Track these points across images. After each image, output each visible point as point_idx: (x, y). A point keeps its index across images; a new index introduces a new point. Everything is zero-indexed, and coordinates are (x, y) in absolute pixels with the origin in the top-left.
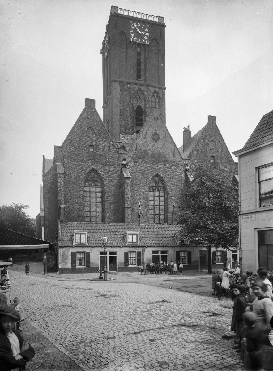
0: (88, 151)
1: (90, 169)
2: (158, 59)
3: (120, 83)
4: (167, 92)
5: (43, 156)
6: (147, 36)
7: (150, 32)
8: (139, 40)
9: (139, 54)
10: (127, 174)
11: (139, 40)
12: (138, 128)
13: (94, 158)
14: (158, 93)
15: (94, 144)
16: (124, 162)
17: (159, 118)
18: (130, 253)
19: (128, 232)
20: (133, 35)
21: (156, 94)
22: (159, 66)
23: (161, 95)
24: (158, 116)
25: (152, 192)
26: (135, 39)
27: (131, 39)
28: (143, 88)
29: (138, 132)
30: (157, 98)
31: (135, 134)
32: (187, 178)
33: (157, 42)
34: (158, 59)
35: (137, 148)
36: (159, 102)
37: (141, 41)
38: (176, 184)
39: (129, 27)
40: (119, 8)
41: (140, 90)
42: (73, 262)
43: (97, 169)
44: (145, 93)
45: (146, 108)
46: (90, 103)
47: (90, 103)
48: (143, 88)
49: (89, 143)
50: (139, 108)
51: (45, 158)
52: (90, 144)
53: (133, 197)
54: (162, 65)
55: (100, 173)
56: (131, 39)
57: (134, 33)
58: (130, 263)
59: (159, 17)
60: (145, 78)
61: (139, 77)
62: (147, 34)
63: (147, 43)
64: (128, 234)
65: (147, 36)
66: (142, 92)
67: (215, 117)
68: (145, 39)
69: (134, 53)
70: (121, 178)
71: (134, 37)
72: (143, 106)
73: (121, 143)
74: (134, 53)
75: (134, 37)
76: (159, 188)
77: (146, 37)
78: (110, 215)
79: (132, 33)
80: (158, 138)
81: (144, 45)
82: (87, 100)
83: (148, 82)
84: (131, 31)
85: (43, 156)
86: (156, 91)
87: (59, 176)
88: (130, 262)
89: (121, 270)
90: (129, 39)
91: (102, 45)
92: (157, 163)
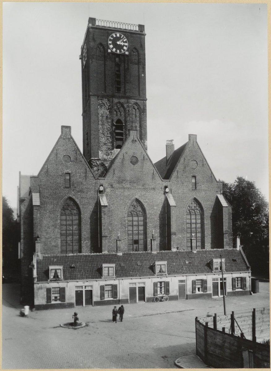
0: (65, 179)
1: (66, 197)
2: (139, 68)
3: (98, 97)
4: (148, 103)
5: (20, 173)
6: (126, 46)
7: (129, 41)
8: (118, 51)
9: (118, 65)
10: (104, 201)
12: (120, 143)
13: (70, 186)
14: (139, 105)
15: (70, 172)
16: (101, 188)
17: (137, 140)
18: (106, 287)
19: (104, 265)
20: (111, 46)
21: (137, 106)
22: (139, 76)
23: (142, 107)
24: (136, 139)
25: (130, 217)
26: (114, 50)
27: (109, 51)
28: (122, 101)
29: (119, 147)
30: (138, 110)
31: (115, 149)
32: (166, 200)
33: (137, 51)
34: (139, 68)
35: (114, 173)
36: (140, 114)
37: (120, 51)
38: (155, 208)
39: (108, 38)
40: (97, 20)
41: (119, 102)
42: (49, 298)
43: (74, 197)
44: (125, 106)
45: (126, 122)
46: (66, 129)
47: (66, 129)
49: (66, 171)
50: (119, 121)
51: (22, 174)
52: (67, 172)
53: (111, 224)
54: (143, 75)
55: (77, 200)
56: (109, 51)
57: (113, 44)
58: (105, 297)
59: (139, 25)
60: (125, 90)
61: (119, 90)
62: (126, 44)
63: (127, 53)
64: (104, 267)
65: (126, 46)
66: (122, 106)
67: (196, 135)
68: (124, 50)
69: (113, 70)
70: (98, 205)
71: (113, 48)
72: (123, 119)
73: (100, 160)
74: (113, 70)
75: (113, 48)
76: (138, 212)
77: (125, 48)
78: (87, 243)
79: (110, 44)
80: (137, 161)
81: (124, 55)
82: (63, 127)
83: (128, 94)
84: (110, 42)
85: (20, 173)
86: (137, 103)
87: (35, 208)
88: (106, 295)
89: (98, 303)
90: (108, 51)
91: (81, 49)
92: (136, 187)
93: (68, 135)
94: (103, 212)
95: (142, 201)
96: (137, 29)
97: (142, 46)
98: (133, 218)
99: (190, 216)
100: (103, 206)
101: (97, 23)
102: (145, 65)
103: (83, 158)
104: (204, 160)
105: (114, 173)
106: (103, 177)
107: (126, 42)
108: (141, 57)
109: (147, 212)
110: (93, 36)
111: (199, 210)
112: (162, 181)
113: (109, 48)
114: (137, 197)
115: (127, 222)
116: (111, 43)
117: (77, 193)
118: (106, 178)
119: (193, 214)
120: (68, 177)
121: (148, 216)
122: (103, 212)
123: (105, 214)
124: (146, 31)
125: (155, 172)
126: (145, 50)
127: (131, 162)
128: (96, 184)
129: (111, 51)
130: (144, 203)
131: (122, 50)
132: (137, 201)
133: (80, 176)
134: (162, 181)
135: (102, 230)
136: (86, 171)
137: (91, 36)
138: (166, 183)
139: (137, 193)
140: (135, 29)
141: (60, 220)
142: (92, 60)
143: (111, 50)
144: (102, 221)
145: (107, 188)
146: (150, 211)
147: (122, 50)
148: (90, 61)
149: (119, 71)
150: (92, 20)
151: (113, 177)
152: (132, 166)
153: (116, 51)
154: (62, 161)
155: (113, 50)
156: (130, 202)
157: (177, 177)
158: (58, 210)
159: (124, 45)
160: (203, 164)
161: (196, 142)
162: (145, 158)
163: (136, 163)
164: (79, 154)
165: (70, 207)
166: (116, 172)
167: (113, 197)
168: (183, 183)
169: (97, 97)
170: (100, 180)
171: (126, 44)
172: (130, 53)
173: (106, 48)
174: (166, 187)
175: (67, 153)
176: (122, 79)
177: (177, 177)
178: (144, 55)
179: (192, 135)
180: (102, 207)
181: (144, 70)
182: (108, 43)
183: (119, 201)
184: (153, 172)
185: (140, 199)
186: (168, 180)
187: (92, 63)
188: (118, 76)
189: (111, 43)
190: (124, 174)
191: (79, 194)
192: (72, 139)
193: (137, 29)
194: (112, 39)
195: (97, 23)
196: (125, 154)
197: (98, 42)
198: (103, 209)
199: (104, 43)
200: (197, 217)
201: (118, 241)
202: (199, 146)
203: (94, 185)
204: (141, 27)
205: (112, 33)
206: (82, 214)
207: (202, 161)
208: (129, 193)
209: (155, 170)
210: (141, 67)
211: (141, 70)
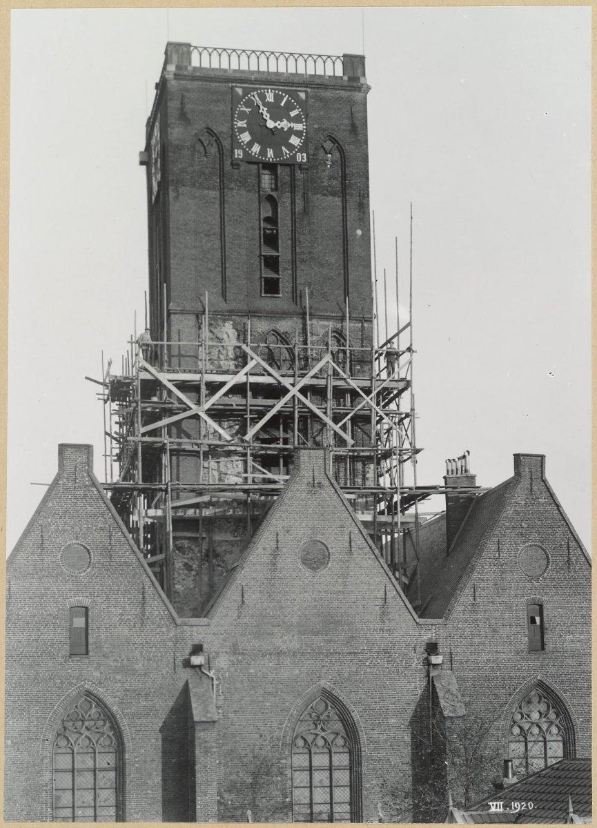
1: (73, 691)
2: (344, 209)
6: (298, 134)
8: (270, 153)
11: (270, 153)
15: (87, 602)
17: (326, 483)
20: (246, 137)
24: (320, 478)
25: (302, 757)
28: (284, 326)
32: (431, 695)
34: (344, 209)
35: (243, 602)
37: (278, 153)
48: (284, 326)
55: (109, 701)
56: (238, 154)
57: (249, 129)
59: (345, 56)
61: (271, 287)
62: (299, 127)
63: (301, 158)
65: (298, 134)
71: (250, 144)
75: (250, 144)
77: (295, 141)
79: (242, 130)
81: (291, 165)
84: (241, 124)
90: (232, 152)
93: (83, 477)
94: (201, 743)
95: (343, 697)
96: (339, 72)
97: (358, 129)
98: (331, 757)
99: (327, 757)
100: (197, 722)
101: (195, 62)
102: (368, 197)
103: (134, 552)
104: (573, 544)
105: (243, 602)
106: (205, 617)
107: (297, 119)
108: (352, 167)
109: (363, 737)
110: (182, 104)
111: (557, 726)
112: (417, 623)
113: (235, 143)
114: (325, 683)
115: (289, 776)
116: (245, 126)
117: (112, 676)
118: (214, 622)
119: (555, 738)
120: (79, 622)
121: (366, 750)
122: (201, 743)
123: (206, 752)
124: (372, 76)
125: (392, 593)
126: (366, 142)
127: (305, 561)
128: (177, 641)
129: (245, 153)
130: (351, 707)
131: (284, 148)
132: (328, 695)
133: (121, 615)
134: (417, 623)
135: (198, 807)
136: (144, 598)
137: (174, 105)
138: (431, 630)
139: (324, 670)
140: (329, 73)
141: (52, 772)
142: (176, 190)
143: (244, 150)
144: (198, 775)
145: (217, 653)
146: (375, 734)
147: (284, 148)
148: (172, 194)
149: (272, 220)
150: (177, 52)
151: (239, 617)
152: (308, 573)
153: (263, 152)
154: (58, 566)
155: (250, 148)
156: (300, 702)
157: (474, 608)
158: (44, 736)
159: (291, 131)
160: (569, 560)
161: (544, 481)
162: (353, 545)
163: (322, 564)
164: (118, 540)
165: (86, 723)
166: (251, 598)
167: (238, 685)
168: (495, 631)
169: (193, 318)
170: (195, 629)
171: (299, 127)
172: (312, 158)
173: (226, 143)
174: (432, 648)
175: (77, 539)
176: (284, 253)
177: (474, 608)
178: (365, 159)
179: (527, 455)
180: (198, 728)
181: (364, 213)
182: (233, 125)
183: (261, 699)
184: (382, 592)
185: (337, 692)
186: (440, 621)
187: (177, 197)
188: (271, 240)
189: (245, 126)
190: (279, 602)
191: (118, 677)
192: (94, 489)
193: (339, 72)
194: (248, 110)
195: (195, 62)
196: (281, 535)
197: (199, 126)
198: (200, 735)
199: (221, 128)
200: (335, 758)
201: (59, 767)
202: (552, 495)
203: (170, 643)
204: (354, 64)
205: (247, 92)
206: (127, 749)
207: (565, 548)
208: (297, 672)
209: (390, 588)
210: (352, 203)
211: (352, 214)
